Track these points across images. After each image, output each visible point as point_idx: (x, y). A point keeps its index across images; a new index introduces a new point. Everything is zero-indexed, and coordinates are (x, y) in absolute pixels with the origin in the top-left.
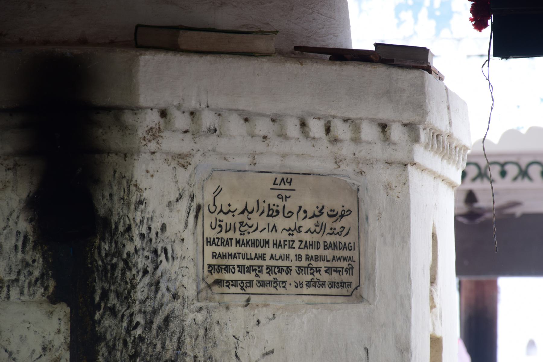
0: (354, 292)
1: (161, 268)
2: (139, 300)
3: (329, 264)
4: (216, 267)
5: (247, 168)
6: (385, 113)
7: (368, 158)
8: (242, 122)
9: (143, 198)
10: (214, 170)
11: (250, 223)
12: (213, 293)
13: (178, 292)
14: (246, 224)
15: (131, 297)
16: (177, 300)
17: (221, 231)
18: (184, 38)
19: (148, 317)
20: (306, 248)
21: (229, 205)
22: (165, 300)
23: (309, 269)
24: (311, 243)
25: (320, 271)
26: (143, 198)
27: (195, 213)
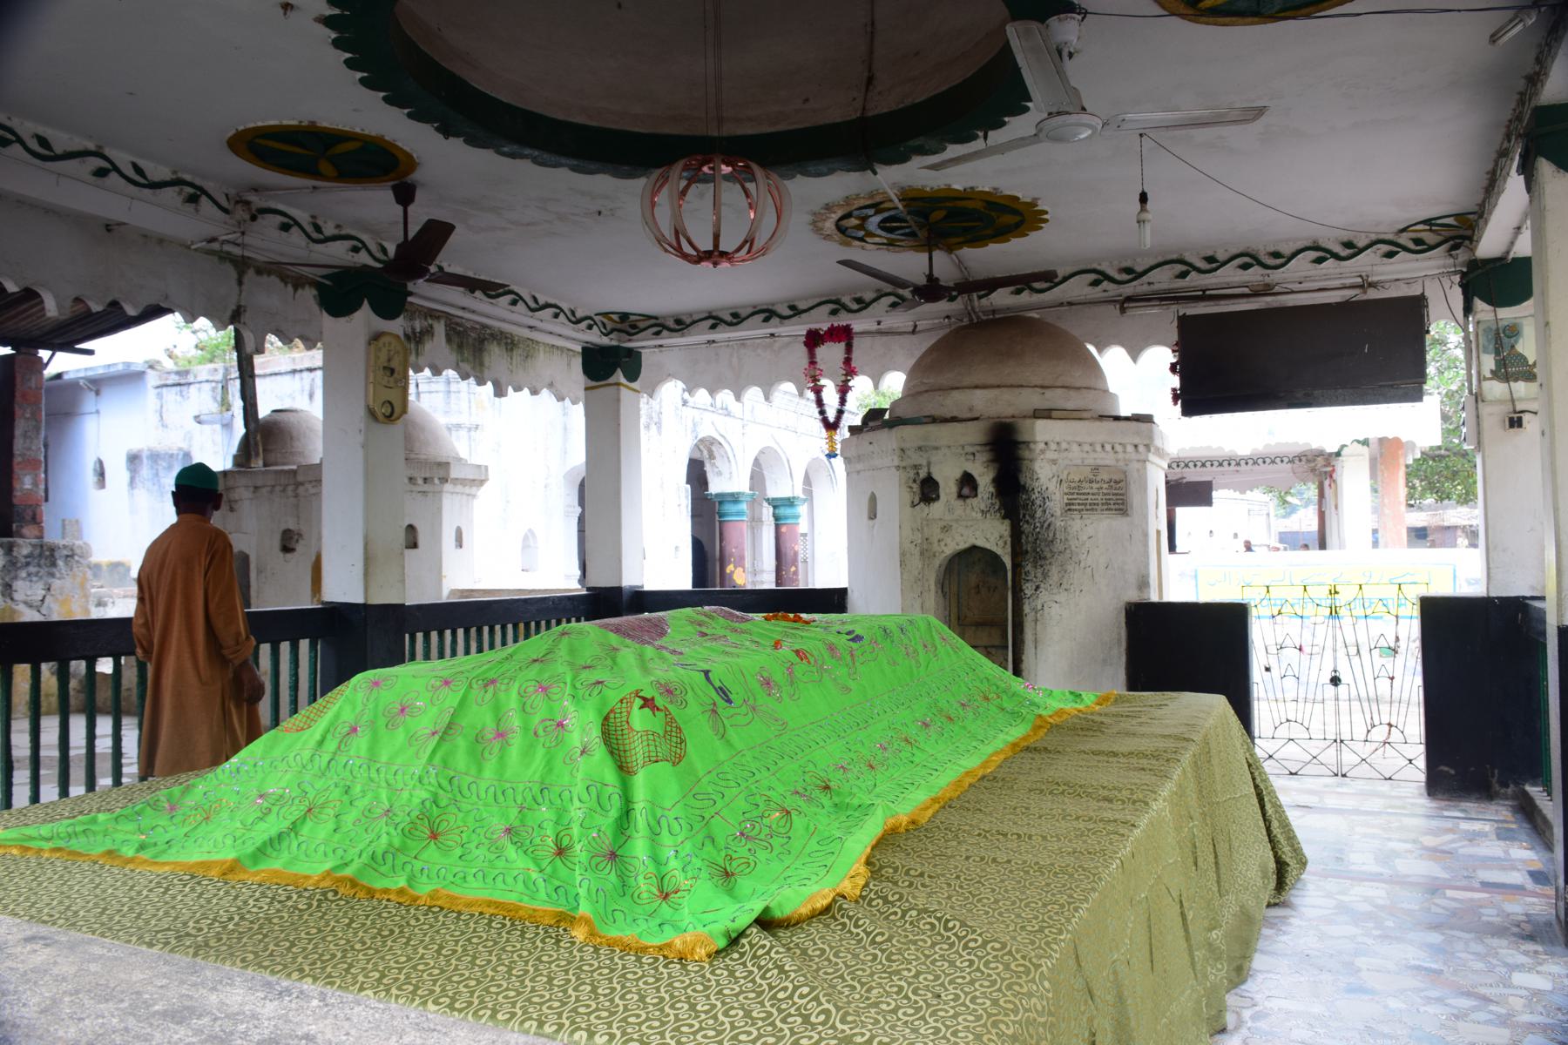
6: (1136, 441)
18: (1054, 414)
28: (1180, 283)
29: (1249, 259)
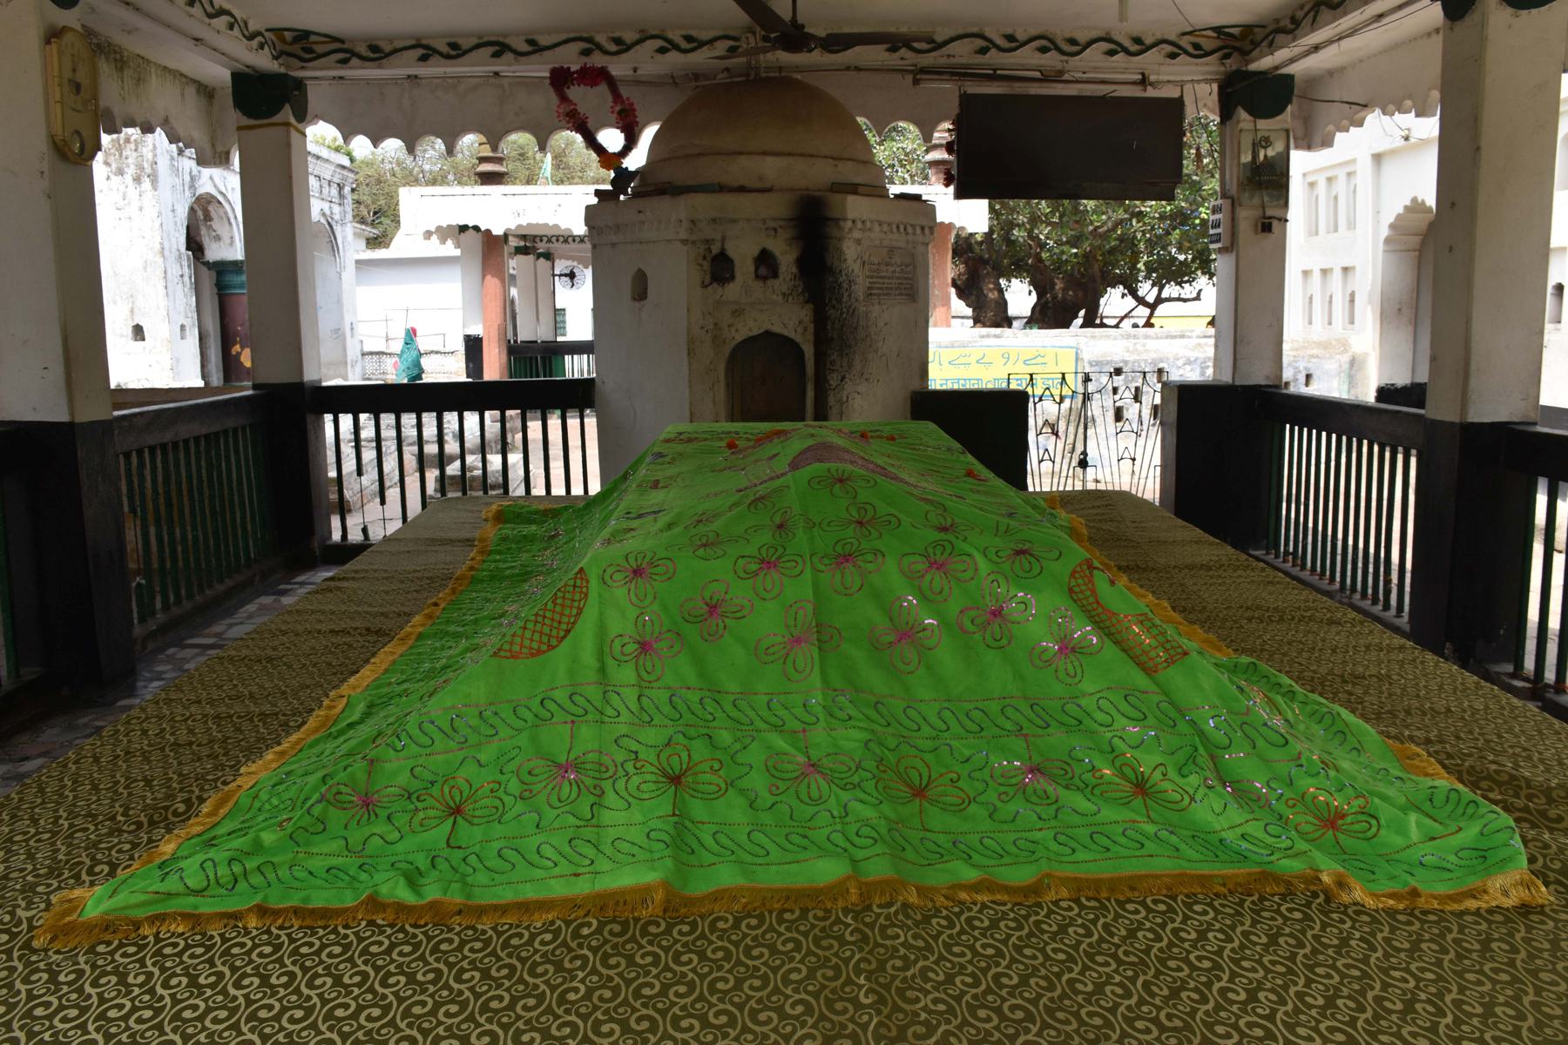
28: (979, 59)
29: (1047, 44)
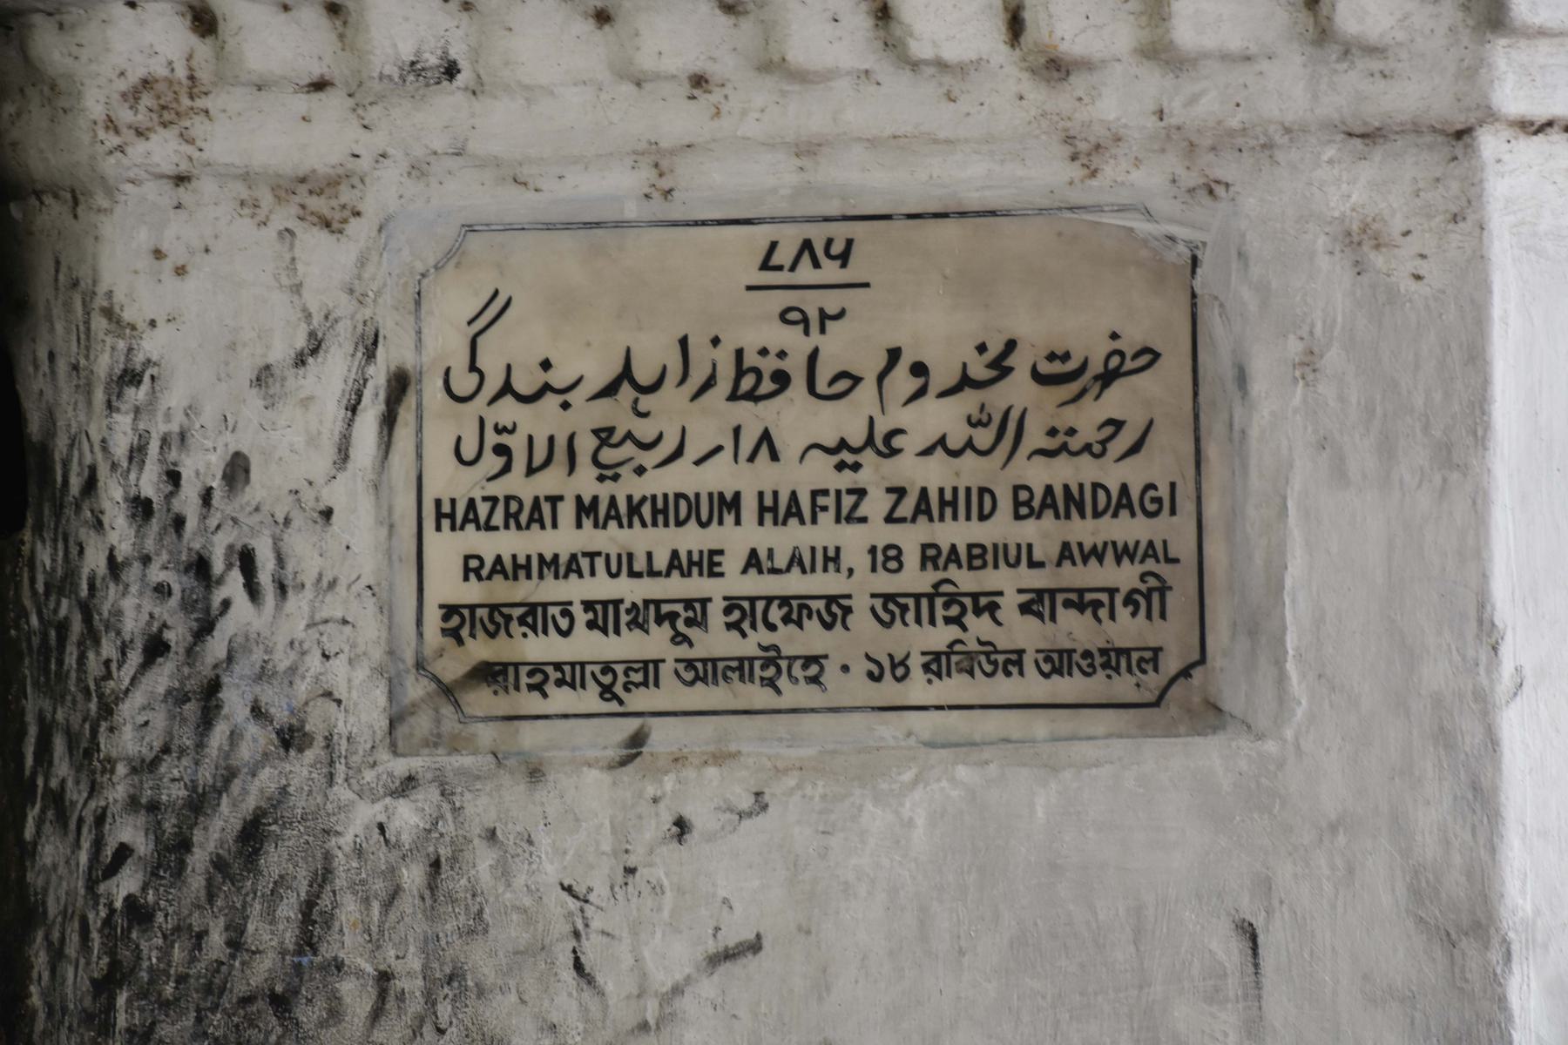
0: (1175, 690)
1: (227, 628)
2: (129, 760)
3: (1038, 579)
4: (482, 613)
5: (631, 211)
7: (1234, 123)
8: (590, 24)
9: (139, 358)
10: (470, 229)
11: (645, 430)
12: (465, 719)
13: (303, 722)
14: (629, 436)
15: (99, 750)
16: (301, 750)
17: (507, 469)
19: (169, 825)
20: (922, 519)
21: (546, 365)
22: (245, 753)
23: (939, 602)
24: (948, 496)
25: (993, 608)
26: (139, 358)
27: (381, 407)
